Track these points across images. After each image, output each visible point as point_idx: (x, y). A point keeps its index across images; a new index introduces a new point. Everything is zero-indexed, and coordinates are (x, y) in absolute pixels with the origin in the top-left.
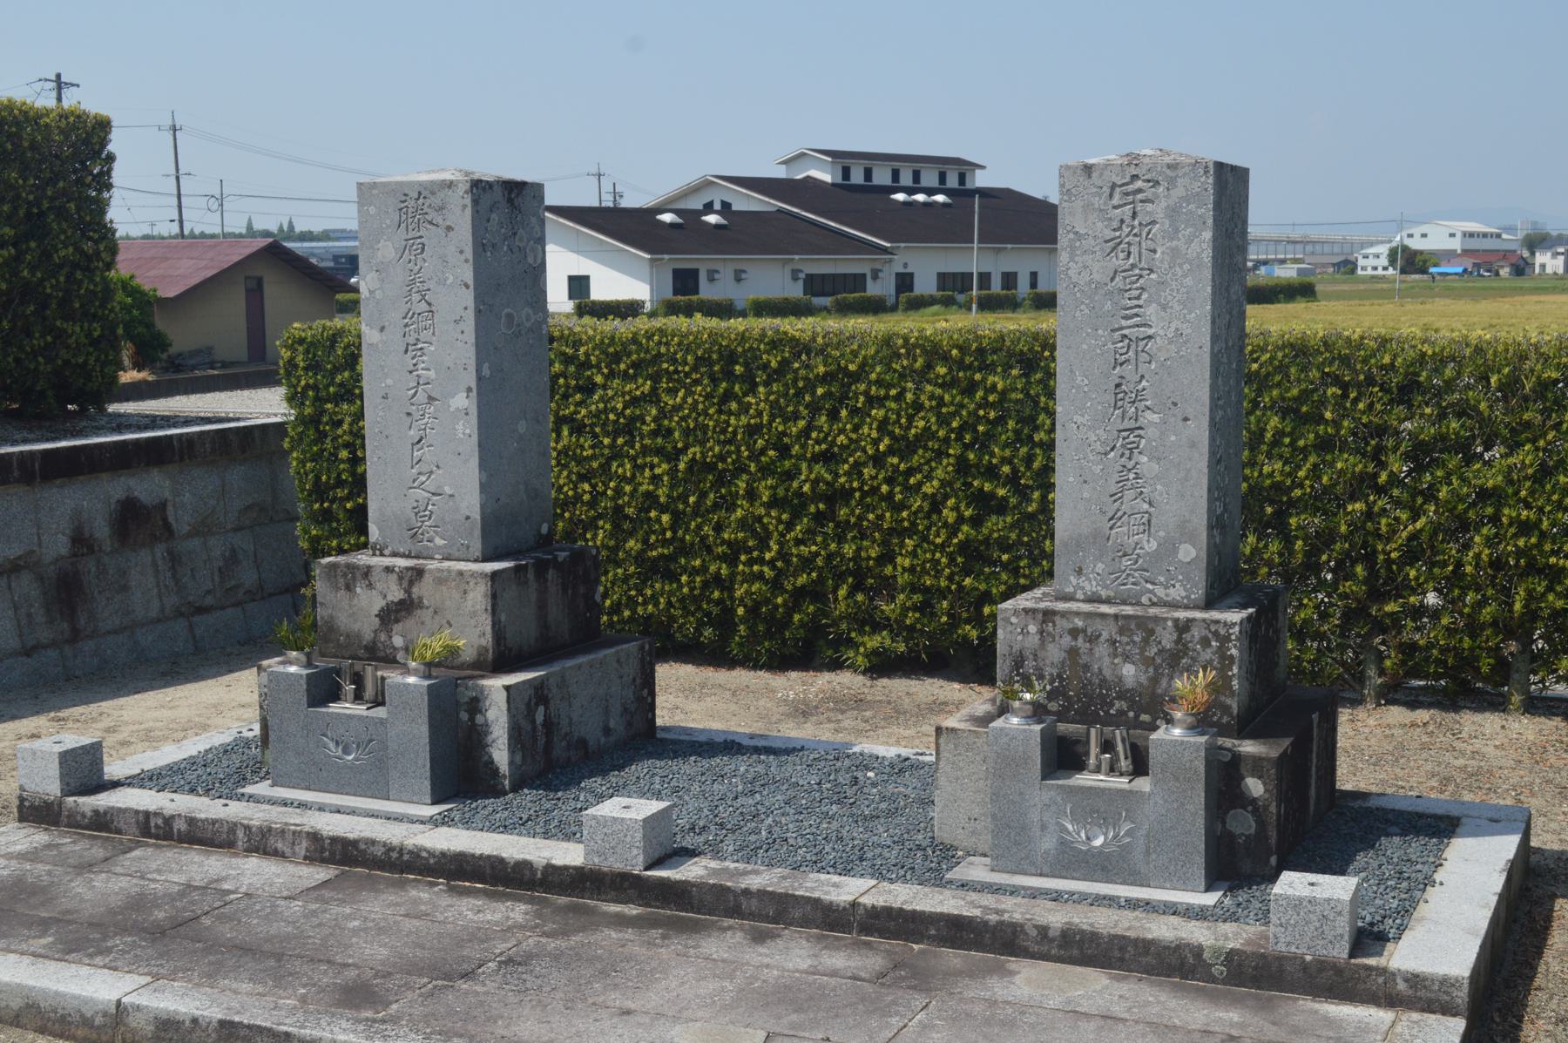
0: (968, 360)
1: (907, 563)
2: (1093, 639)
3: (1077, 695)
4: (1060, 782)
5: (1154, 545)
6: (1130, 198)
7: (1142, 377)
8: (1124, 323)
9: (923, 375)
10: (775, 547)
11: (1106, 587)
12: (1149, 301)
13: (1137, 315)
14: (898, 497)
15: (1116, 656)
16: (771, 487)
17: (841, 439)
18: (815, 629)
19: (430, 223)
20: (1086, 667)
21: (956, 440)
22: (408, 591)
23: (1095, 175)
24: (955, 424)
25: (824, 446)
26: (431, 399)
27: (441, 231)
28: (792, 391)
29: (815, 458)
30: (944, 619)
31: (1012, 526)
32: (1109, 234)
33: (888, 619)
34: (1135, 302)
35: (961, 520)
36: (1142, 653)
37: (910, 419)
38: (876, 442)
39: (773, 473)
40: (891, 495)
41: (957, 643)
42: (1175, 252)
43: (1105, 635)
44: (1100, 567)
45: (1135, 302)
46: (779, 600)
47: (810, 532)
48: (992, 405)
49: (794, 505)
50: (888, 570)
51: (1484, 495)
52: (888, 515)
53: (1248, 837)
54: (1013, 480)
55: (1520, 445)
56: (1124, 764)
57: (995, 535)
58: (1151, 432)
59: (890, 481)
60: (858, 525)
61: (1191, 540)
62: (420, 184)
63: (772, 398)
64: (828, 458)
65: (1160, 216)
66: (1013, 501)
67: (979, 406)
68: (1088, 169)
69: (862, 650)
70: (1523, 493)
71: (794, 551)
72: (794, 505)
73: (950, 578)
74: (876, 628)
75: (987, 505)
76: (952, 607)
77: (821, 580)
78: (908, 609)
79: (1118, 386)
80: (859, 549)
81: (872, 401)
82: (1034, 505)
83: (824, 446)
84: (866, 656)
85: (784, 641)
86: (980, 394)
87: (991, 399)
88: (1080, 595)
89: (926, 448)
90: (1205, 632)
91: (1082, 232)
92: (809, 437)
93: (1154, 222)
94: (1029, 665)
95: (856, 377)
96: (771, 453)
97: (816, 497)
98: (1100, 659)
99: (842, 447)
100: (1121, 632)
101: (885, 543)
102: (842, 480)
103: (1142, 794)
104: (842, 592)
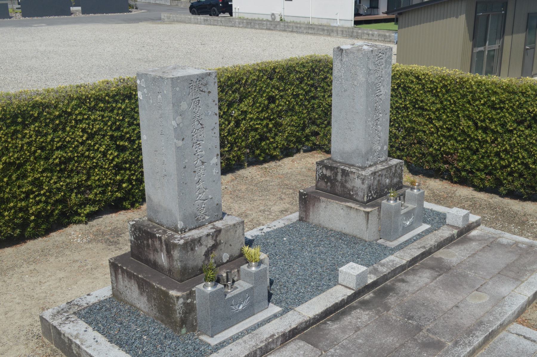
17: (68, 139)
18: (63, 214)
19: (202, 91)
22: (215, 240)
26: (203, 163)
27: (206, 94)
62: (197, 75)
81: (77, 122)
83: (60, 143)
92: (54, 141)
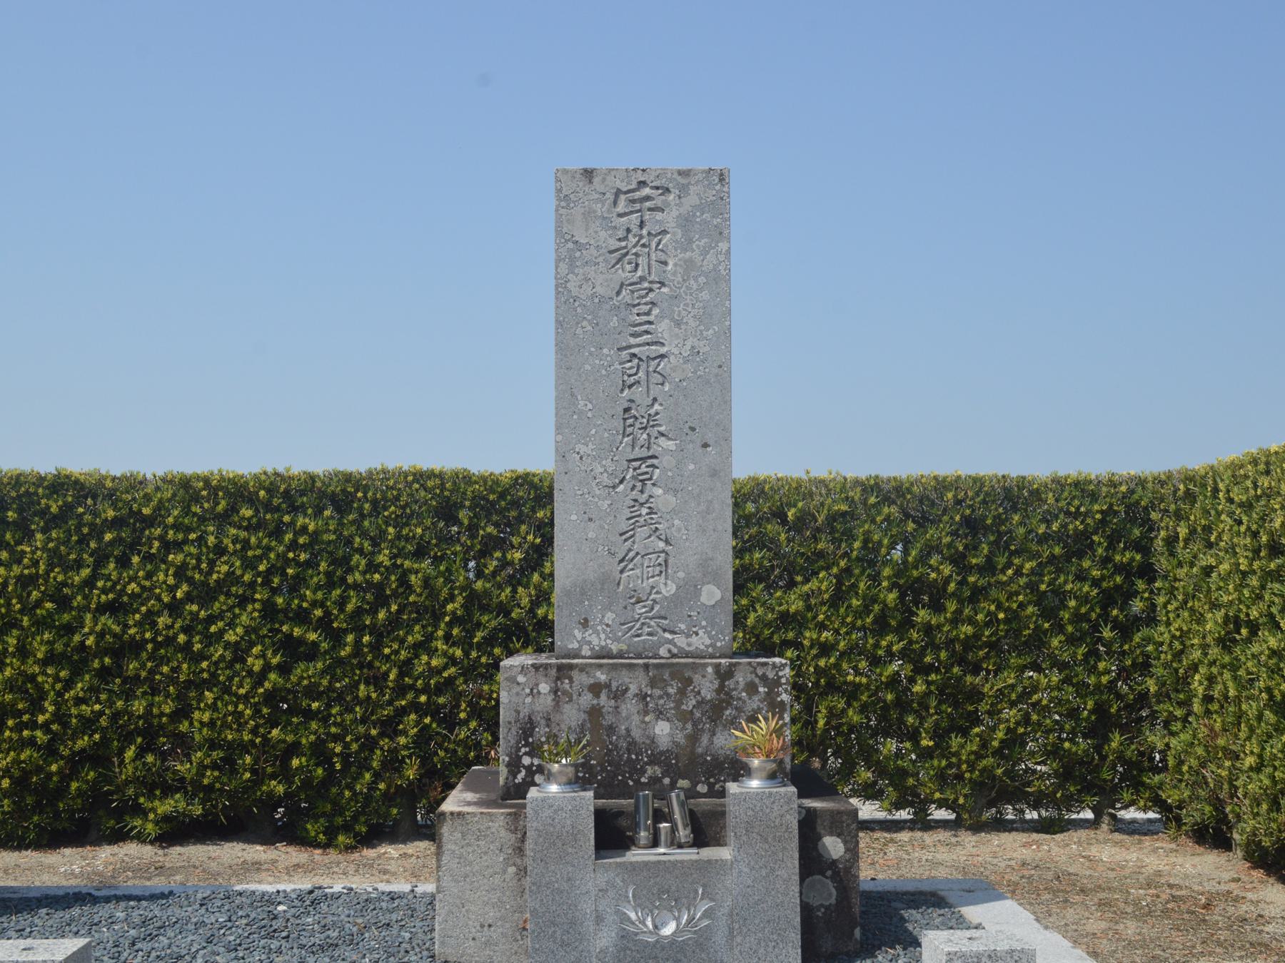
0: (276, 501)
1: (206, 717)
2: (619, 695)
3: (601, 764)
4: (618, 860)
5: (672, 588)
6: (637, 206)
7: (655, 400)
8: (633, 341)
9: (224, 519)
10: (51, 709)
11: (617, 640)
12: (661, 317)
13: (647, 332)
14: (197, 647)
15: (646, 713)
16: (48, 642)
18: (96, 798)
20: (611, 729)
21: (263, 584)
23: (596, 180)
24: (262, 568)
25: (111, 596)
28: (74, 538)
29: (102, 609)
30: (248, 775)
31: (323, 672)
32: (614, 244)
33: (182, 779)
34: (645, 318)
35: (267, 668)
36: (677, 707)
37: (212, 564)
38: (172, 589)
39: (50, 627)
40: (189, 644)
41: (261, 800)
42: (689, 264)
43: (633, 689)
44: (609, 618)
45: (645, 318)
46: (54, 768)
47: (93, 690)
48: (304, 547)
49: (77, 661)
50: (184, 727)
51: (786, 619)
52: (185, 666)
53: (827, 908)
54: (324, 625)
55: (816, 573)
56: (684, 833)
57: (305, 682)
58: (666, 461)
59: (185, 630)
60: (149, 678)
61: (716, 579)
63: (51, 545)
64: (114, 608)
65: (671, 225)
66: (325, 646)
67: (289, 549)
68: (589, 174)
69: (151, 816)
70: (821, 617)
71: (74, 711)
72: (77, 661)
73: (254, 731)
74: (168, 791)
75: (295, 651)
76: (256, 760)
77: (105, 742)
78: (206, 767)
79: (627, 410)
80: (151, 705)
81: (167, 546)
82: (348, 649)
83: (111, 596)
84: (156, 823)
85: (57, 814)
86: (288, 537)
87: (301, 541)
88: (586, 651)
89: (228, 595)
90: (750, 677)
91: (583, 241)
93: (664, 232)
94: (541, 732)
95: (150, 522)
96: (49, 605)
97: (101, 652)
98: (627, 718)
99: (133, 596)
100: (653, 683)
101: (180, 697)
102: (132, 631)
103: (723, 862)
104: (130, 753)
